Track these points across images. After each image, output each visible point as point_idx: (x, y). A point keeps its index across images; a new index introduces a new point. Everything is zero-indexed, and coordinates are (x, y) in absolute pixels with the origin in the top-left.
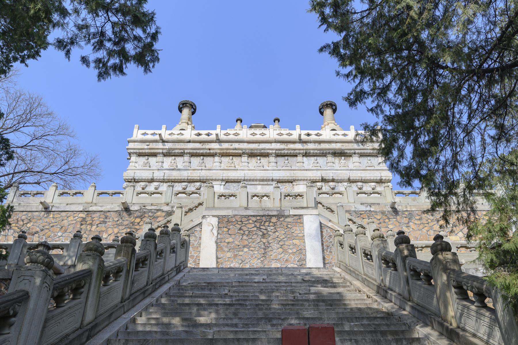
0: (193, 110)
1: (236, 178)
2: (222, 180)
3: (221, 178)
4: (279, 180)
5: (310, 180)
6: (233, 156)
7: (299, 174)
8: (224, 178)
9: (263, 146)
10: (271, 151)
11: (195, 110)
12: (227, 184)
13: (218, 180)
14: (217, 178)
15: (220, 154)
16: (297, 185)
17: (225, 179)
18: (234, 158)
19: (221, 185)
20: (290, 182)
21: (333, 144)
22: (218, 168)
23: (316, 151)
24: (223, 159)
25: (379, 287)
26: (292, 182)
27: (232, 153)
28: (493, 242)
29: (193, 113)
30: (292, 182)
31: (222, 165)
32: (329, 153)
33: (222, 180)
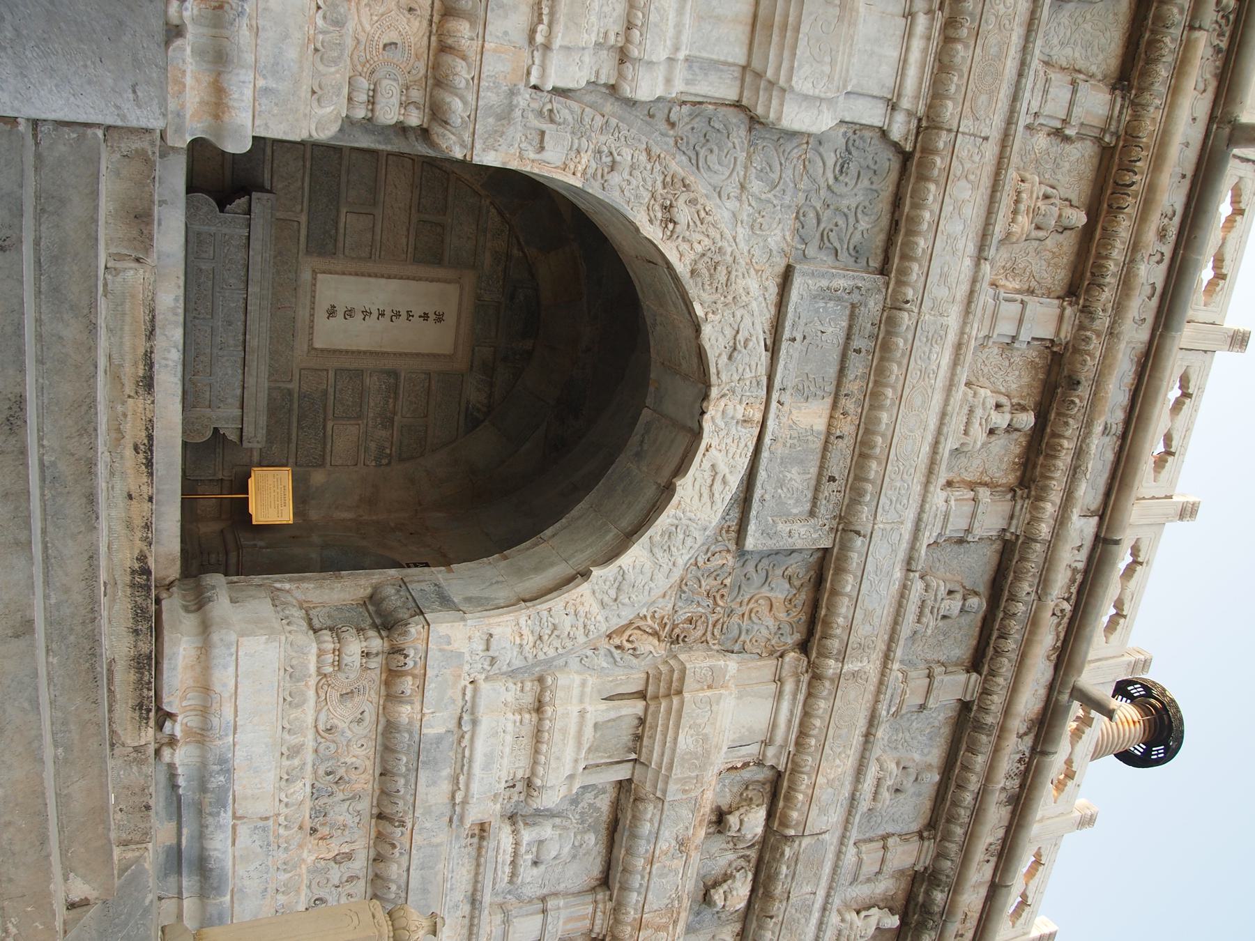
0: (1139, 750)
1: (922, 243)
2: (927, 125)
3: (950, 110)
4: (840, 570)
5: (795, 769)
6: (1087, 233)
7: (847, 708)
8: (942, 141)
9: (1100, 451)
10: (1050, 509)
11: (1142, 761)
12: (888, 162)
13: (937, 94)
14: (954, 84)
15: (1130, 136)
16: (779, 680)
17: (928, 150)
18: (1068, 242)
19: (893, 106)
20: (810, 632)
21: (988, 871)
22: (1030, 100)
23: (974, 783)
24: (1080, 156)
25: (199, 609)
26: (804, 647)
27: (1108, 236)
28: (605, 665)
29: (1126, 757)
30: (804, 647)
31: (1041, 141)
32: (940, 855)
33: (927, 125)
